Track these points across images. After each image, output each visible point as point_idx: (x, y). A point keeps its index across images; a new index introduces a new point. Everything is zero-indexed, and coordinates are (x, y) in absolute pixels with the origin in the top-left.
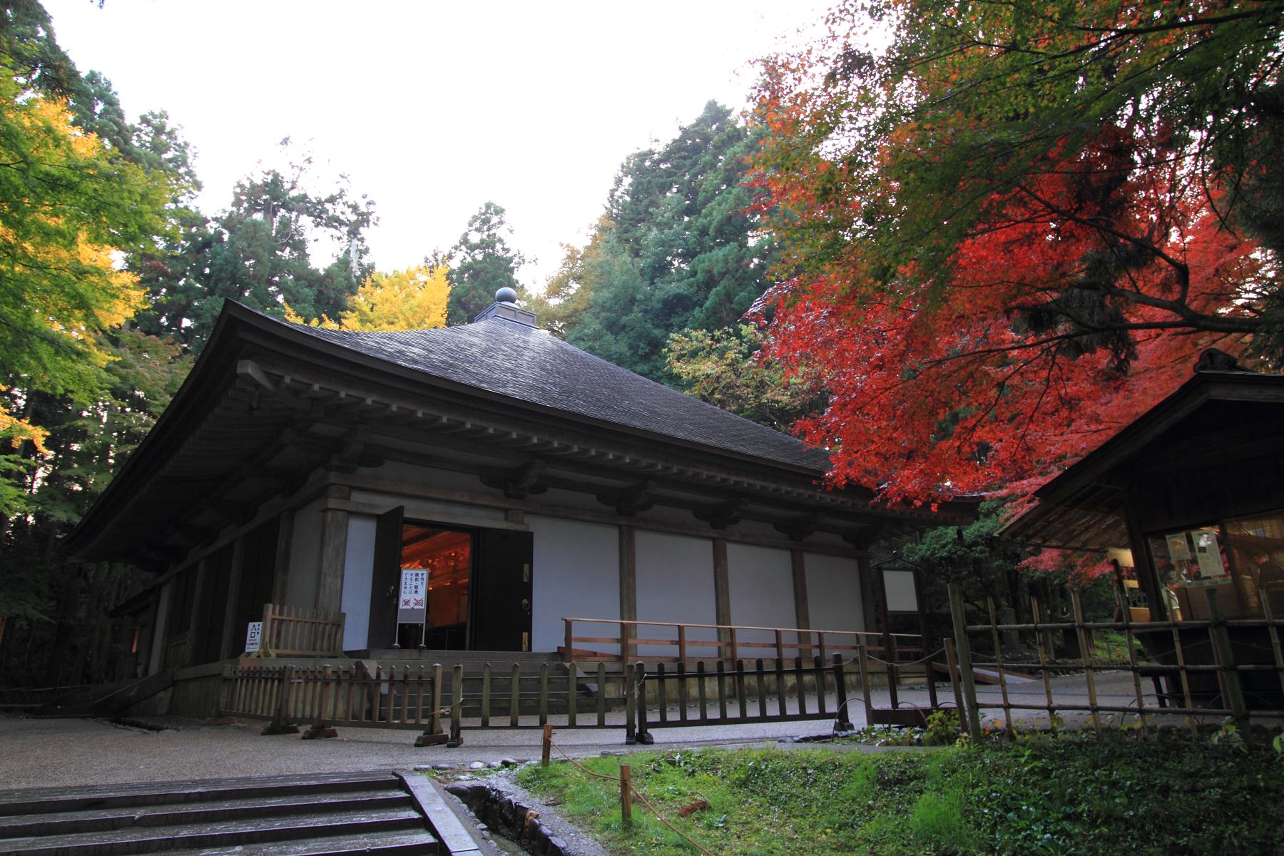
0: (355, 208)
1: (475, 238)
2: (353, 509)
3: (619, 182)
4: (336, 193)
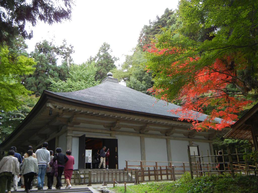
0: (68, 49)
1: (102, 54)
2: (73, 135)
3: (142, 35)
4: (62, 45)
